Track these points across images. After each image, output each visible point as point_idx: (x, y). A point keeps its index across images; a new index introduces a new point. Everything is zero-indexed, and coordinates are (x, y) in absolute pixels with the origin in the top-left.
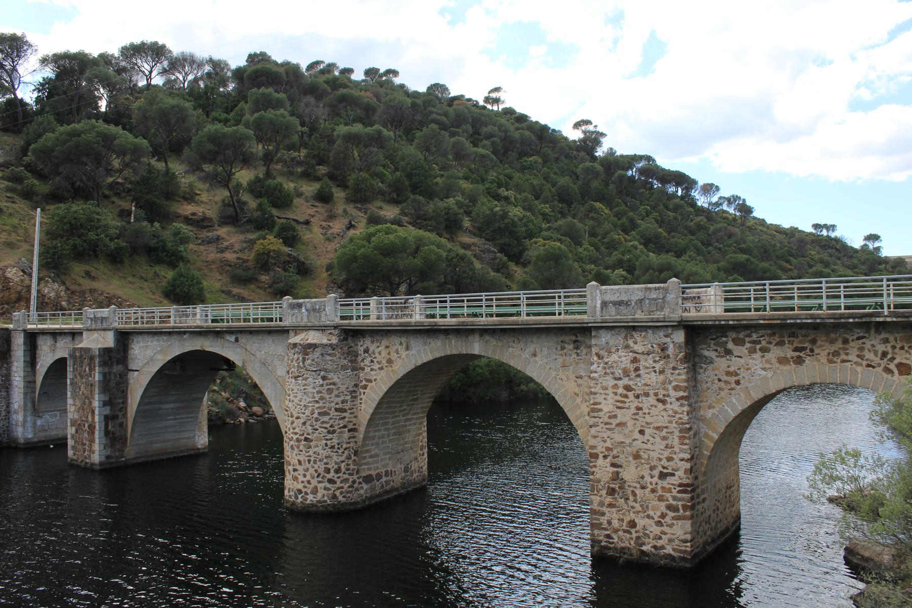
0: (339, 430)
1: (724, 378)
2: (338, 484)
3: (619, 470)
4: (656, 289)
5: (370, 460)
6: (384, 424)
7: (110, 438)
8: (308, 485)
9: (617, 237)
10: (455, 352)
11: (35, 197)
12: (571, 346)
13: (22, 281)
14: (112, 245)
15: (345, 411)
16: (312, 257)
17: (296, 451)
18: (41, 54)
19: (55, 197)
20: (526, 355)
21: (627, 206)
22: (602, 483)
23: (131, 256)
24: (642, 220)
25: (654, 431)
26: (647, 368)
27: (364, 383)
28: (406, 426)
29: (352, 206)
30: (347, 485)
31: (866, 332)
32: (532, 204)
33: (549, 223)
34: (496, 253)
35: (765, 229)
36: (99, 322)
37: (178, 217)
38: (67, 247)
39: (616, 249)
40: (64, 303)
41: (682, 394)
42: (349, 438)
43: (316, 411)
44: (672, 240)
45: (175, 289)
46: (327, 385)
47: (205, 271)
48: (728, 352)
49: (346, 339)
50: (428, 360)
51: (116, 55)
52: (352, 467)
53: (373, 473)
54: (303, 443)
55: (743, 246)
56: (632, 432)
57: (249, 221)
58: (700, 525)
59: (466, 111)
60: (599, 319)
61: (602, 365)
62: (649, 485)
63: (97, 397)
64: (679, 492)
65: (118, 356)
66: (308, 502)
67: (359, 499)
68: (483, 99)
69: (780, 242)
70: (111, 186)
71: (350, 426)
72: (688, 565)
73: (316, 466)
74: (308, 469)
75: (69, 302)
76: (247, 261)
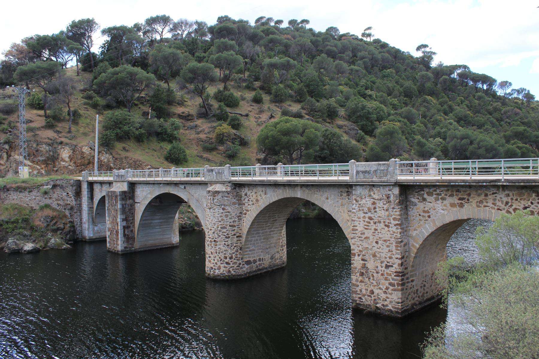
0: (232, 237)
1: (422, 214)
2: (231, 265)
3: (366, 262)
4: (383, 164)
5: (250, 252)
6: (257, 234)
7: (126, 238)
8: (216, 265)
9: (439, 117)
10: (288, 196)
11: (98, 107)
12: (345, 194)
13: (90, 153)
15: (235, 226)
16: (249, 135)
17: (210, 247)
18: (102, 28)
19: (108, 107)
20: (323, 198)
23: (148, 138)
25: (383, 242)
26: (380, 207)
27: (245, 212)
28: (271, 234)
30: (236, 265)
31: (497, 190)
32: (386, 99)
33: (396, 110)
36: (120, 177)
38: (113, 135)
39: (438, 125)
40: (112, 165)
41: (397, 222)
42: (237, 241)
43: (220, 227)
44: (476, 118)
45: (171, 156)
46: (225, 213)
48: (424, 200)
49: (235, 188)
50: (275, 200)
52: (238, 256)
53: (252, 259)
54: (213, 243)
55: (526, 120)
56: (372, 242)
57: (214, 116)
58: (409, 294)
59: (348, 43)
60: (355, 180)
61: (357, 205)
62: (380, 271)
63: (119, 216)
64: (395, 276)
65: (130, 195)
66: (216, 274)
67: (243, 273)
70: (139, 99)
71: (238, 235)
72: (400, 316)
73: (220, 255)
74: (216, 257)
75: (114, 164)
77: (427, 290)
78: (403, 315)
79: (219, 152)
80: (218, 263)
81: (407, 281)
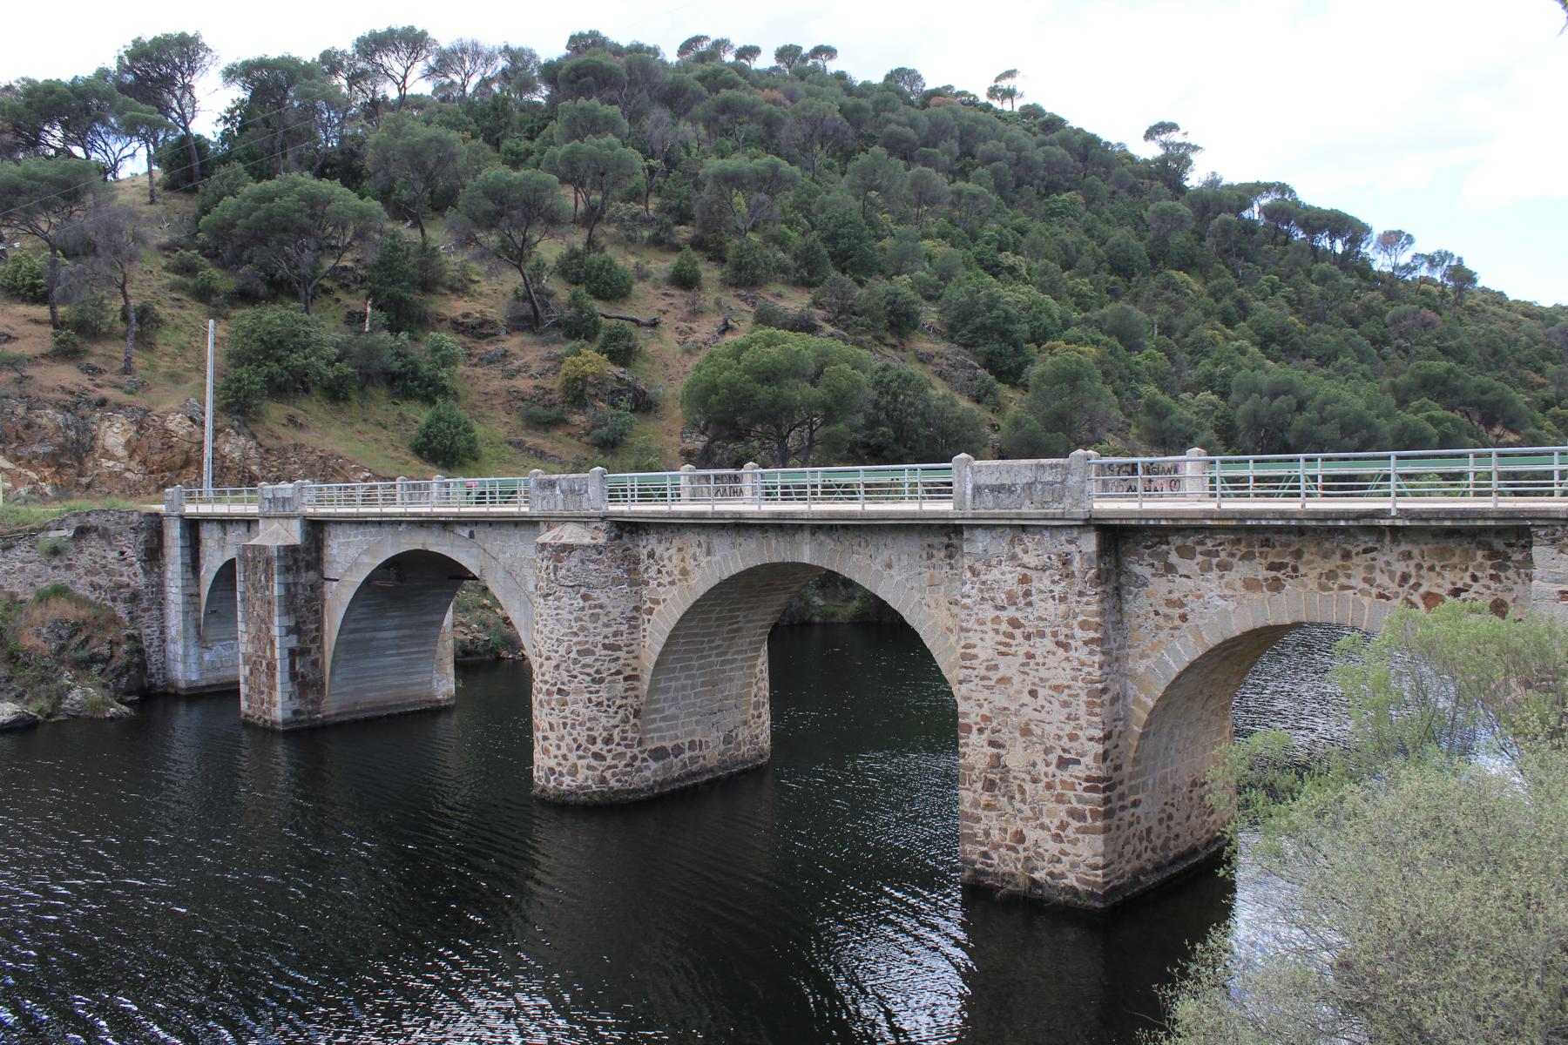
0: (610, 678)
1: (1164, 610)
2: (609, 762)
3: (1001, 751)
4: (1052, 467)
5: (663, 724)
6: (682, 669)
9: (1210, 332)
10: (775, 559)
11: (213, 298)
12: (942, 554)
14: (331, 373)
15: (619, 648)
17: (546, 709)
19: (245, 296)
20: (878, 566)
21: (1236, 276)
22: (977, 771)
23: (362, 388)
24: (1264, 300)
25: (1051, 692)
26: (1042, 592)
27: (648, 604)
28: (725, 671)
29: (731, 292)
30: (623, 763)
31: (1378, 541)
33: (1085, 311)
34: (976, 369)
35: (1502, 311)
36: (280, 504)
37: (441, 321)
38: (257, 379)
39: (1206, 355)
40: (254, 468)
41: (1092, 634)
42: (626, 690)
43: (575, 649)
46: (590, 608)
47: (484, 410)
48: (1170, 568)
49: (619, 537)
51: (350, 51)
53: (668, 745)
54: (556, 696)
56: (1019, 692)
57: (557, 325)
60: (969, 512)
61: (977, 586)
62: (1043, 777)
63: (276, 620)
64: (1086, 789)
65: (308, 558)
66: (564, 787)
67: (642, 785)
68: (986, 91)
69: (1529, 335)
70: (335, 273)
71: (628, 672)
72: (1099, 905)
73: (575, 733)
75: (262, 467)
76: (551, 391)
77: (1177, 829)
78: (1110, 902)
79: (573, 430)
80: (570, 756)
81: (1120, 803)
